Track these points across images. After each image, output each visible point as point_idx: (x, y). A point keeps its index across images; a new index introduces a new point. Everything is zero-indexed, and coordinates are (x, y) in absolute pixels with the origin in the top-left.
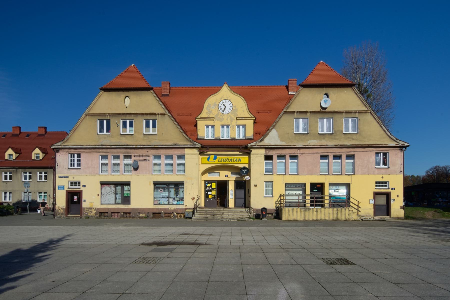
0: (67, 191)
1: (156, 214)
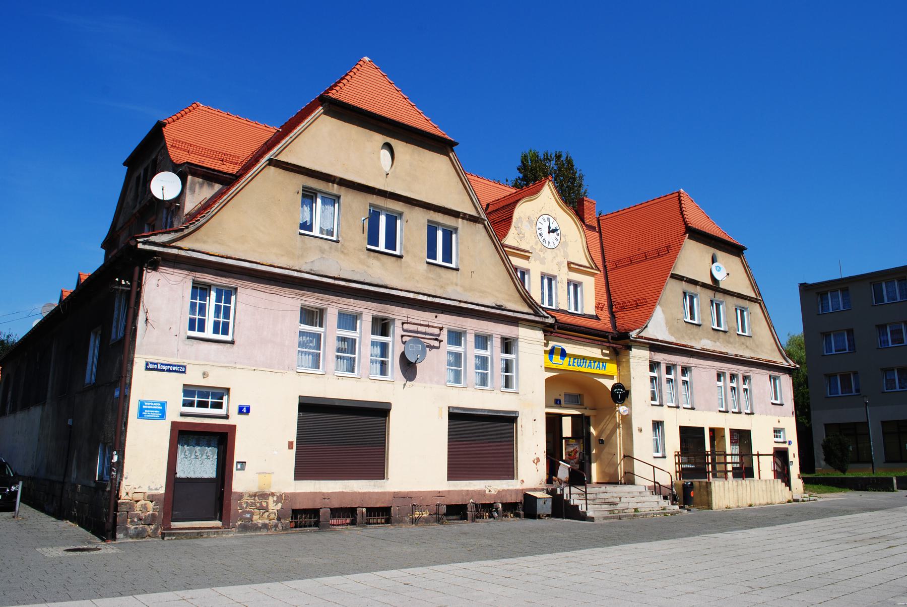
0: (174, 424)
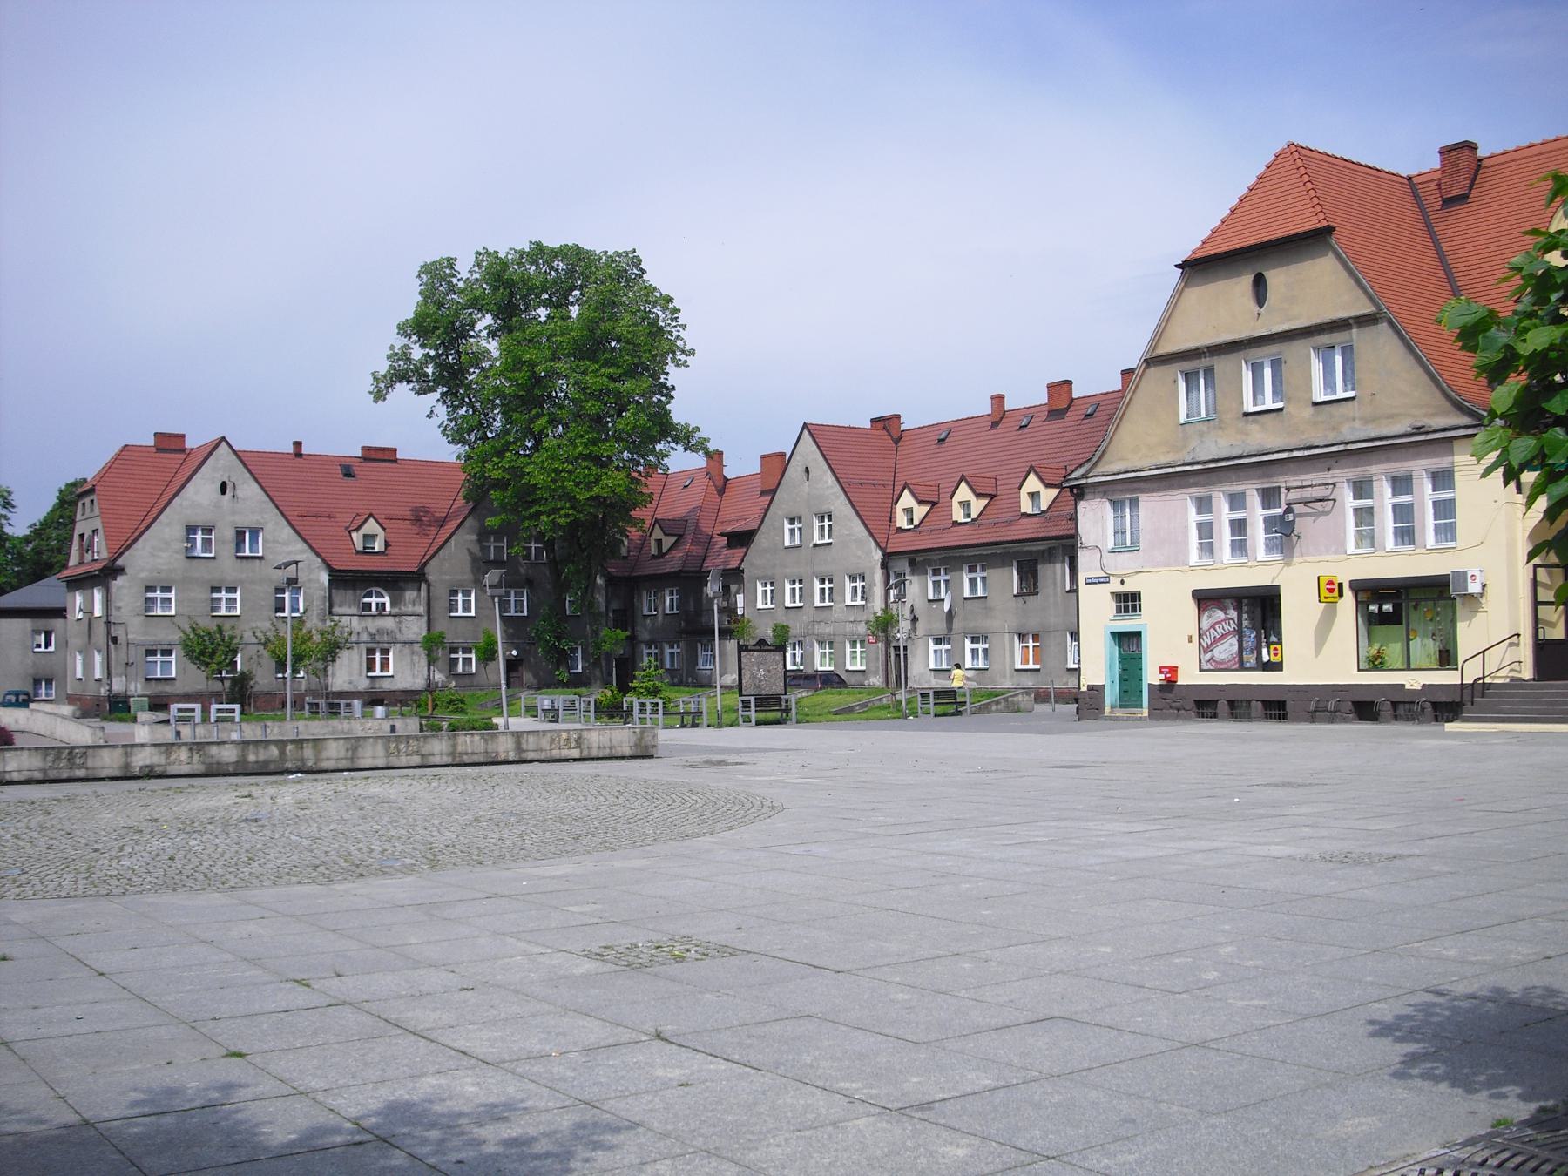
1: (1363, 707)
